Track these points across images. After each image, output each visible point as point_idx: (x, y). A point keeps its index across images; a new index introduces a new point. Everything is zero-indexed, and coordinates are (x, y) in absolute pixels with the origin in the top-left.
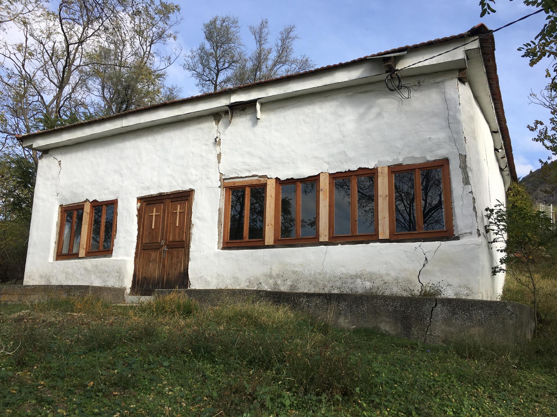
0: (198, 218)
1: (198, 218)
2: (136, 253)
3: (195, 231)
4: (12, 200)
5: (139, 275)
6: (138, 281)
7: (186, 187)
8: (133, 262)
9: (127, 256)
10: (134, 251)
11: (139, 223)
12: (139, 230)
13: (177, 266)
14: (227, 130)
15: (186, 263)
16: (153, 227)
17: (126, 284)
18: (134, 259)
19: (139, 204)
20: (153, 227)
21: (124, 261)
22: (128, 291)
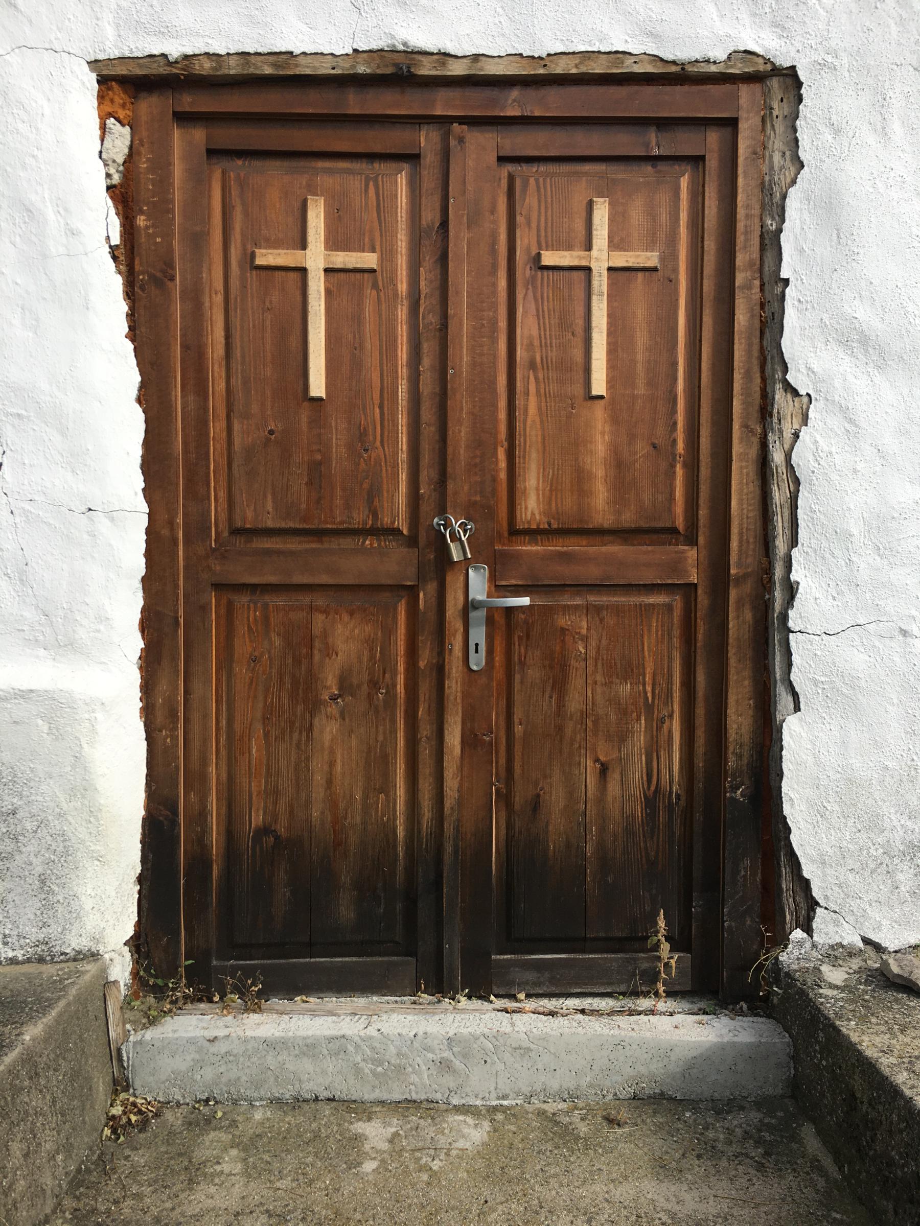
0: (856, 341)
1: (856, 341)
2: (152, 623)
3: (819, 451)
4: (761, 994)
5: (200, 817)
6: (200, 862)
7: (707, 33)
8: (135, 703)
9: (65, 646)
10: (129, 604)
11: (144, 329)
12: (151, 396)
13: (622, 737)
14: (86, 68)
15: (739, 721)
16: (318, 387)
17: (91, 922)
18: (135, 678)
19: (121, 139)
20: (599, 386)
21: (55, 708)
22: (121, 969)
